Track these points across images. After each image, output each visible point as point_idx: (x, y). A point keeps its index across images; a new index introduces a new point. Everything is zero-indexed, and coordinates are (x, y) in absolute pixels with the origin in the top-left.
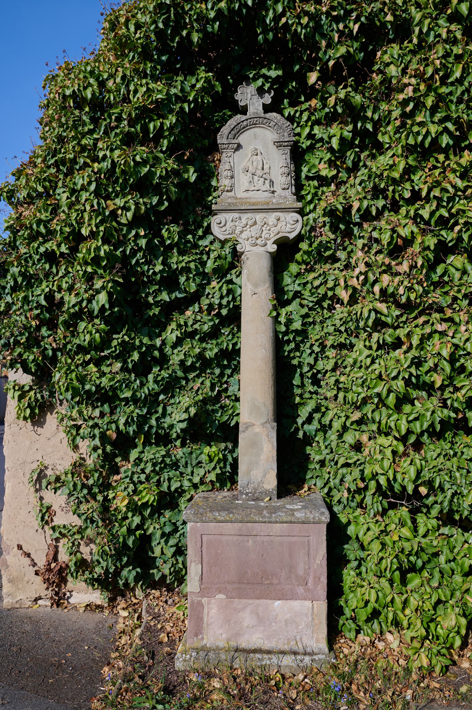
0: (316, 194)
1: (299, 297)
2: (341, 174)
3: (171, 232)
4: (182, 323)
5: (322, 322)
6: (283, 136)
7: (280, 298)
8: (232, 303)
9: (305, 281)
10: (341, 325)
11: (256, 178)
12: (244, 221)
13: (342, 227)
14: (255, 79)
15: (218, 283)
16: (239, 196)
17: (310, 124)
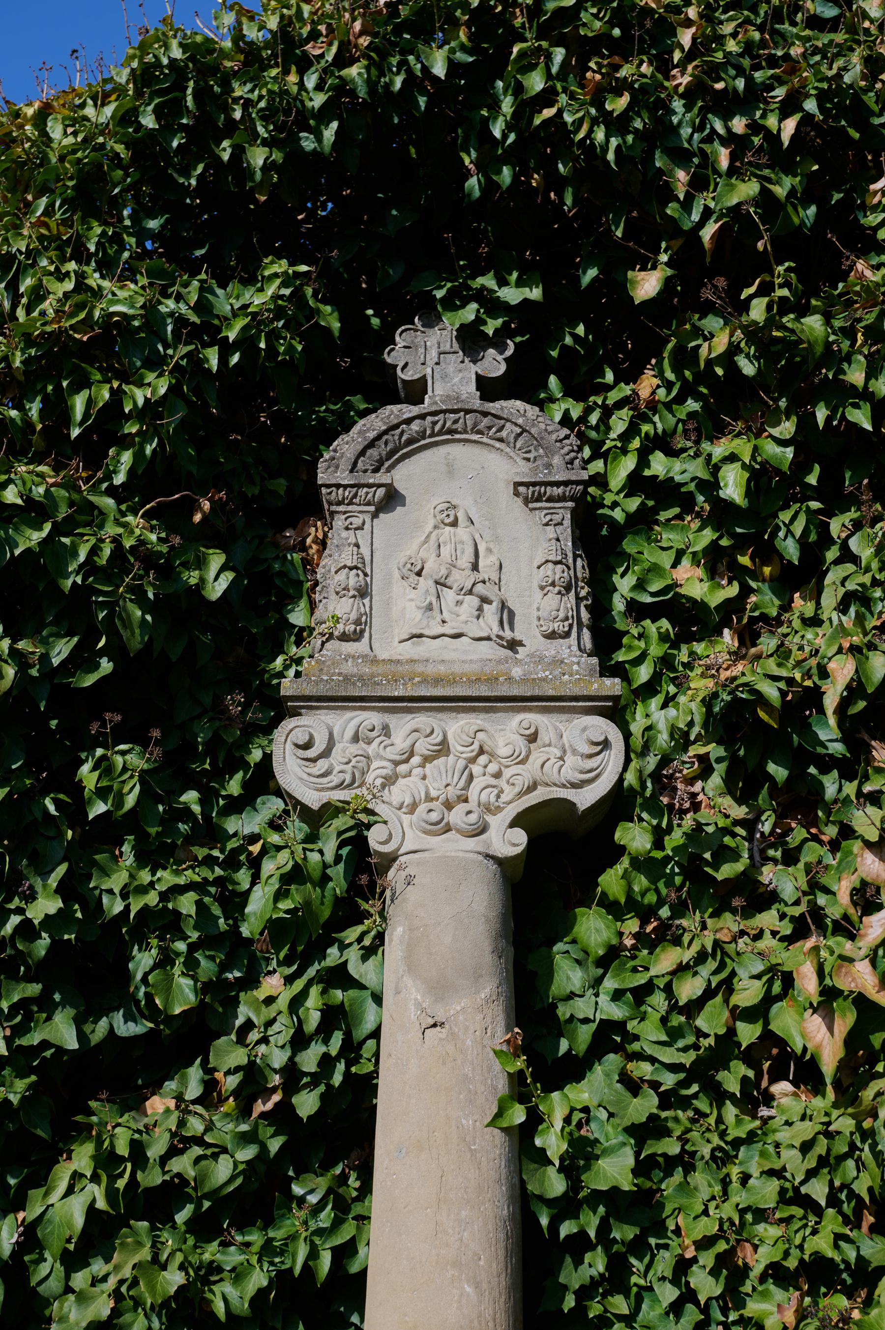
0: (666, 662)
1: (618, 1049)
2: (753, 599)
3: (115, 773)
4: (123, 1150)
5: (721, 1158)
6: (549, 466)
7: (542, 1049)
8: (341, 1067)
9: (641, 979)
10: (811, 1174)
11: (449, 596)
12: (400, 741)
13: (778, 771)
14: (453, 302)
15: (289, 980)
16: (383, 655)
17: (636, 443)
